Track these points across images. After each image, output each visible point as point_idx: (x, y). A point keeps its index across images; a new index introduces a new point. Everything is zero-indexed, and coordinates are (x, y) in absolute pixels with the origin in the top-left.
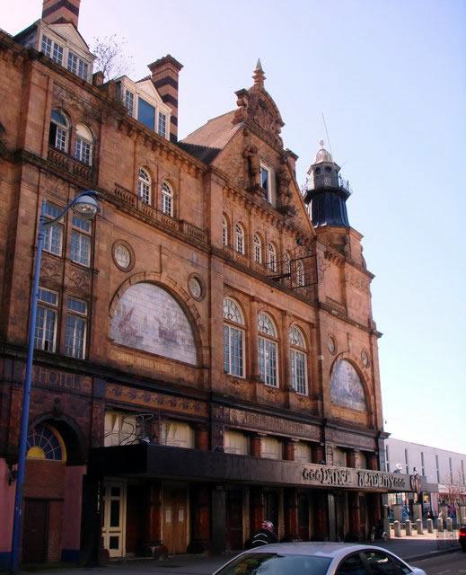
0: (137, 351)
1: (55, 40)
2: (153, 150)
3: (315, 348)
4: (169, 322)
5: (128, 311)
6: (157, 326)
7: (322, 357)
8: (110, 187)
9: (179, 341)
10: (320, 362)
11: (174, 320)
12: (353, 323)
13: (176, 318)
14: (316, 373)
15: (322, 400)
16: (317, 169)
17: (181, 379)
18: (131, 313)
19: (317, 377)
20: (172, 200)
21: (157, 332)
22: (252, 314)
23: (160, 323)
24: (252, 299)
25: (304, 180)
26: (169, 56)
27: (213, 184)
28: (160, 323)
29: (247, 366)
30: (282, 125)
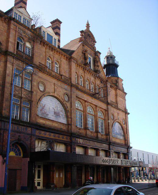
0: (46, 119)
1: (18, 13)
2: (52, 51)
3: (107, 118)
4: (57, 109)
5: (43, 105)
6: (53, 111)
7: (109, 121)
8: (37, 64)
9: (61, 116)
10: (109, 123)
11: (59, 109)
12: (120, 110)
13: (60, 108)
14: (107, 126)
15: (109, 136)
16: (107, 57)
17: (61, 129)
18: (44, 106)
19: (107, 128)
20: (58, 68)
21: (53, 113)
22: (85, 107)
23: (54, 110)
24: (86, 101)
25: (103, 61)
26: (57, 19)
27: (72, 63)
28: (54, 110)
29: (84, 124)
30: (96, 42)
